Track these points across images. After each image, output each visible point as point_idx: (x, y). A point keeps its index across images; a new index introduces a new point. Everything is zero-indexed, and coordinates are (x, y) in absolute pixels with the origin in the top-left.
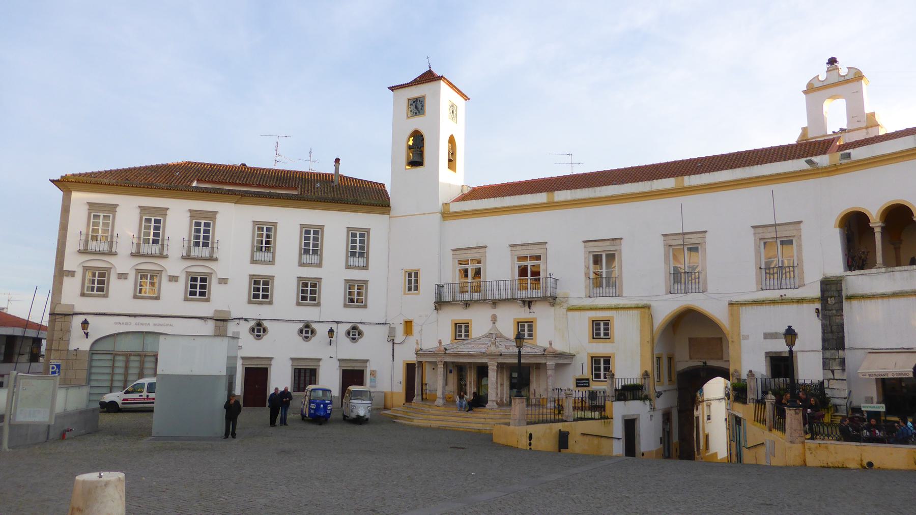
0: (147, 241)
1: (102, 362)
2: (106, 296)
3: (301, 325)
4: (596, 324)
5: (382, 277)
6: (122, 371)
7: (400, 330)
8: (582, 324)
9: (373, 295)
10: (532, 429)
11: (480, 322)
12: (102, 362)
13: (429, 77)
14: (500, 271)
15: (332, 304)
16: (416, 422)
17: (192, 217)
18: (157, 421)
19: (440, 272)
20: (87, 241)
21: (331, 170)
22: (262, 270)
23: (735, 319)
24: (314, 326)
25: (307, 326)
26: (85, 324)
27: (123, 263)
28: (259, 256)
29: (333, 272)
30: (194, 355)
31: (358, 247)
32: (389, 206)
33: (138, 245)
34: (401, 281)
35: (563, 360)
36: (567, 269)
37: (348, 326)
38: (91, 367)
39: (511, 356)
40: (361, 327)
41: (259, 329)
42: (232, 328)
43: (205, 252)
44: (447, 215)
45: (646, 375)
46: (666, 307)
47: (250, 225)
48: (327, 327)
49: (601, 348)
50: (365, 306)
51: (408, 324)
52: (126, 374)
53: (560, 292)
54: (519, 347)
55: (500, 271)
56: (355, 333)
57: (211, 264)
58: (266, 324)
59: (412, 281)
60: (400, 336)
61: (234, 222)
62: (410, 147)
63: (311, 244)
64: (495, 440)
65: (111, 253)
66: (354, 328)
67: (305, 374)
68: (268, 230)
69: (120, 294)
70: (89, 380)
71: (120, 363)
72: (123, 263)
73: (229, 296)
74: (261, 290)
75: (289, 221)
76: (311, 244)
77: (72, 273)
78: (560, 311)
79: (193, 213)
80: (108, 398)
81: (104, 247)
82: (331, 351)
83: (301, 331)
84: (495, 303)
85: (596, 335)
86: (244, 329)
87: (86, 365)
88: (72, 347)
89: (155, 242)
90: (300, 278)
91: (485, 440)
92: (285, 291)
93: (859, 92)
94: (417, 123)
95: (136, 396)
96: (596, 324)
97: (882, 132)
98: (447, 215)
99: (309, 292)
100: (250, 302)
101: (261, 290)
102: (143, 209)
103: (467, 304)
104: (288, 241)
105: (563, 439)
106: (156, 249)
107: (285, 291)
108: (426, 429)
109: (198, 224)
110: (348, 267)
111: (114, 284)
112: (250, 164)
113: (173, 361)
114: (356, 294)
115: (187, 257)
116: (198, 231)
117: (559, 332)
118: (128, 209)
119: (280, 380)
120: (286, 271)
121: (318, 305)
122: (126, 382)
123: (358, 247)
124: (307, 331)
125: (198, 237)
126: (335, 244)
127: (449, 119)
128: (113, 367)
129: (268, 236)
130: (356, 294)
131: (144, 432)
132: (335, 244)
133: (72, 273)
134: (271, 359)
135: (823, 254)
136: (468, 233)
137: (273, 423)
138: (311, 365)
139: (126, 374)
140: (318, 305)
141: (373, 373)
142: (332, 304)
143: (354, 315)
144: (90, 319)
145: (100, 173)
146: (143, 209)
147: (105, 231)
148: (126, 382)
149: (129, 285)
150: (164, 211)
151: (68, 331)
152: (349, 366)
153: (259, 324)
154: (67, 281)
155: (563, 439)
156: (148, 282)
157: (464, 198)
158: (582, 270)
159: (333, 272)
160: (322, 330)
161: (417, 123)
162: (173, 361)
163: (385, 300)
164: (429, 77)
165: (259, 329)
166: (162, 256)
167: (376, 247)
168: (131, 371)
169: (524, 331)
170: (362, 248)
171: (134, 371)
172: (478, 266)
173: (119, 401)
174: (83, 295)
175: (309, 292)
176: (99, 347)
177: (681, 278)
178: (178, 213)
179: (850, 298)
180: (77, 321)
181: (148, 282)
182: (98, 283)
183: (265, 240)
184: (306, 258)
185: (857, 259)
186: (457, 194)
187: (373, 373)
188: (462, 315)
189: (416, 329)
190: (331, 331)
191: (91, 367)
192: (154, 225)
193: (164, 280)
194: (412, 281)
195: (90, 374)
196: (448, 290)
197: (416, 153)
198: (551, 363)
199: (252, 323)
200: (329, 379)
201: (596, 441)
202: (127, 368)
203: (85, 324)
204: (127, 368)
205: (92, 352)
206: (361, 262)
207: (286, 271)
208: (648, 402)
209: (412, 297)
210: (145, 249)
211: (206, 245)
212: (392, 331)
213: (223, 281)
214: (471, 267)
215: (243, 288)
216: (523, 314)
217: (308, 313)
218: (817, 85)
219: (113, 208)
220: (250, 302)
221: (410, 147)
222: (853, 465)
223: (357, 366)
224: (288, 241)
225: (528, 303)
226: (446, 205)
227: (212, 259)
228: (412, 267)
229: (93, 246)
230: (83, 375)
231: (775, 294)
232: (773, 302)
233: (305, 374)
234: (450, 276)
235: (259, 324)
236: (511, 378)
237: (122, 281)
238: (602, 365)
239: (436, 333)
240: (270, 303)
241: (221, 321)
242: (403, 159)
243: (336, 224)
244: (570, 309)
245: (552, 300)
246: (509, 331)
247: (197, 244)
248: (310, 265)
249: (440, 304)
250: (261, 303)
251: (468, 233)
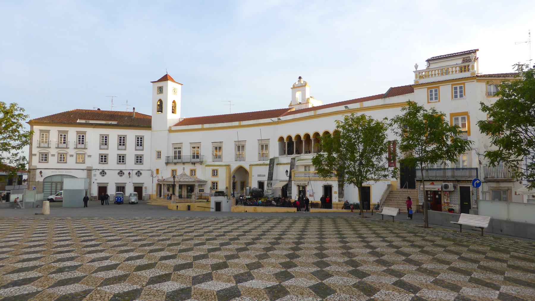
0: (61, 143)
1: (48, 186)
2: (48, 162)
3: (119, 171)
4: (213, 171)
5: (148, 153)
6: (55, 188)
7: (155, 172)
8: (209, 170)
9: (145, 160)
10: (178, 204)
11: (180, 169)
12: (48, 186)
13: (165, 78)
14: (186, 152)
15: (130, 163)
16: (153, 204)
17: (77, 134)
18: (64, 203)
19: (168, 152)
20: (40, 143)
21: (132, 111)
22: (104, 152)
23: (251, 169)
24: (123, 171)
25: (121, 171)
26: (41, 172)
27: (53, 151)
28: (102, 147)
29: (130, 152)
30: (75, 184)
31: (140, 142)
32: (151, 127)
33: (58, 144)
34: (155, 155)
35: (202, 183)
36: (207, 152)
37: (136, 171)
38: (44, 187)
39: (171, 182)
40: (141, 171)
41: (103, 173)
42: (93, 172)
43: (83, 146)
44: (170, 131)
45: (227, 188)
46: (234, 166)
47: (99, 136)
48: (128, 172)
49: (215, 179)
50: (143, 164)
51: (158, 170)
52: (56, 189)
53: (204, 160)
54: (174, 179)
55: (186, 152)
56: (139, 173)
57: (84, 150)
58: (105, 171)
59: (159, 155)
60: (155, 175)
61: (93, 135)
62: (158, 105)
63: (122, 141)
64: (169, 208)
65: (48, 147)
66: (139, 172)
67: (121, 188)
68: (106, 137)
69: (53, 162)
70: (43, 192)
71: (54, 186)
72: (53, 151)
73: (93, 162)
74: (104, 159)
75: (114, 134)
76: (122, 141)
77: (35, 155)
78: (203, 166)
79: (78, 132)
80: (50, 197)
81: (46, 145)
82: (130, 180)
83: (119, 173)
84: (184, 163)
85: (214, 175)
86: (98, 172)
87: (42, 187)
88: (37, 180)
89: (64, 143)
90: (118, 155)
91: (166, 208)
92: (112, 159)
93: (305, 90)
94: (160, 96)
95: (60, 196)
96: (213, 171)
97: (310, 106)
98: (170, 131)
99: (121, 159)
100: (100, 163)
101: (104, 159)
102: (59, 131)
103: (175, 164)
104: (113, 141)
105: (189, 208)
106: (65, 145)
107: (112, 159)
108: (156, 205)
109: (80, 136)
110: (136, 150)
111: (50, 158)
112: (102, 109)
113: (68, 185)
114: (139, 159)
115: (76, 148)
116: (80, 138)
117: (203, 174)
118: (54, 131)
119: (111, 191)
120: (113, 151)
121: (125, 164)
122: (56, 192)
123: (140, 142)
124: (121, 173)
125: (80, 141)
126: (131, 142)
127: (173, 92)
128: (52, 187)
129: (106, 139)
130: (139, 159)
131: (61, 206)
132: (131, 142)
133: (35, 155)
134: (108, 183)
135: (274, 150)
136: (177, 138)
137: (102, 204)
138: (123, 185)
139: (56, 189)
140: (125, 164)
141: (146, 188)
142: (130, 163)
143: (139, 167)
144: (42, 170)
145: (43, 118)
146: (59, 131)
147: (46, 139)
148: (56, 192)
149: (55, 159)
150: (67, 132)
151: (35, 175)
152: (137, 185)
153: (103, 171)
154: (33, 157)
155: (189, 208)
156: (62, 158)
157: (176, 125)
158: (211, 152)
159: (130, 152)
160: (126, 173)
161: (160, 96)
162: (68, 185)
163: (150, 161)
164: (165, 78)
165: (103, 173)
166: (67, 148)
167: (146, 142)
168: (58, 188)
169: (193, 172)
170: (141, 143)
171: (59, 188)
172: (179, 150)
173: (54, 198)
174: (39, 162)
175: (121, 159)
176: (46, 180)
177: (239, 157)
178: (72, 133)
179: (277, 164)
180: (38, 172)
181: (62, 158)
182: (45, 158)
183: (105, 140)
184: (120, 147)
185: (282, 153)
186: (177, 122)
187: (146, 188)
188: (174, 167)
189: (160, 172)
190: (129, 173)
191: (44, 187)
192: (63, 138)
193: (68, 156)
194: (159, 155)
195: (44, 189)
196: (171, 158)
197: (160, 108)
198: (196, 184)
199: (101, 171)
200: (129, 190)
201: (203, 209)
202: (56, 187)
203: (41, 172)
204: (56, 187)
205: (44, 182)
206: (141, 148)
207: (113, 151)
208: (226, 197)
209: (159, 161)
210: (60, 146)
211: (83, 143)
212: (152, 172)
213: (90, 156)
214: (177, 150)
215: (97, 158)
216: (192, 167)
217: (121, 167)
218: (296, 86)
219: (48, 131)
220: (100, 163)
221: (158, 105)
222: (243, 211)
223: (140, 185)
224: (113, 141)
225: (194, 163)
226: (170, 127)
227: (85, 148)
228: (159, 150)
229: (42, 145)
230: (41, 190)
231: (261, 162)
232: (260, 165)
233: (121, 188)
234: (171, 154)
235: (103, 171)
236: (187, 189)
237: (72, 157)
238: (215, 185)
239: (166, 174)
240: (107, 163)
241: (89, 170)
242: (156, 110)
243: (131, 134)
244: (206, 166)
245: (201, 163)
246: (188, 173)
247: (43, 142)
248: (122, 149)
249: (167, 163)
250: (103, 164)
251: (177, 138)
